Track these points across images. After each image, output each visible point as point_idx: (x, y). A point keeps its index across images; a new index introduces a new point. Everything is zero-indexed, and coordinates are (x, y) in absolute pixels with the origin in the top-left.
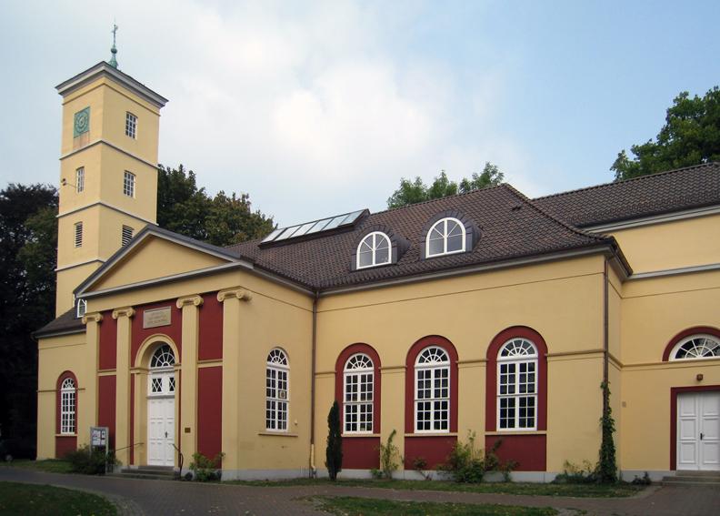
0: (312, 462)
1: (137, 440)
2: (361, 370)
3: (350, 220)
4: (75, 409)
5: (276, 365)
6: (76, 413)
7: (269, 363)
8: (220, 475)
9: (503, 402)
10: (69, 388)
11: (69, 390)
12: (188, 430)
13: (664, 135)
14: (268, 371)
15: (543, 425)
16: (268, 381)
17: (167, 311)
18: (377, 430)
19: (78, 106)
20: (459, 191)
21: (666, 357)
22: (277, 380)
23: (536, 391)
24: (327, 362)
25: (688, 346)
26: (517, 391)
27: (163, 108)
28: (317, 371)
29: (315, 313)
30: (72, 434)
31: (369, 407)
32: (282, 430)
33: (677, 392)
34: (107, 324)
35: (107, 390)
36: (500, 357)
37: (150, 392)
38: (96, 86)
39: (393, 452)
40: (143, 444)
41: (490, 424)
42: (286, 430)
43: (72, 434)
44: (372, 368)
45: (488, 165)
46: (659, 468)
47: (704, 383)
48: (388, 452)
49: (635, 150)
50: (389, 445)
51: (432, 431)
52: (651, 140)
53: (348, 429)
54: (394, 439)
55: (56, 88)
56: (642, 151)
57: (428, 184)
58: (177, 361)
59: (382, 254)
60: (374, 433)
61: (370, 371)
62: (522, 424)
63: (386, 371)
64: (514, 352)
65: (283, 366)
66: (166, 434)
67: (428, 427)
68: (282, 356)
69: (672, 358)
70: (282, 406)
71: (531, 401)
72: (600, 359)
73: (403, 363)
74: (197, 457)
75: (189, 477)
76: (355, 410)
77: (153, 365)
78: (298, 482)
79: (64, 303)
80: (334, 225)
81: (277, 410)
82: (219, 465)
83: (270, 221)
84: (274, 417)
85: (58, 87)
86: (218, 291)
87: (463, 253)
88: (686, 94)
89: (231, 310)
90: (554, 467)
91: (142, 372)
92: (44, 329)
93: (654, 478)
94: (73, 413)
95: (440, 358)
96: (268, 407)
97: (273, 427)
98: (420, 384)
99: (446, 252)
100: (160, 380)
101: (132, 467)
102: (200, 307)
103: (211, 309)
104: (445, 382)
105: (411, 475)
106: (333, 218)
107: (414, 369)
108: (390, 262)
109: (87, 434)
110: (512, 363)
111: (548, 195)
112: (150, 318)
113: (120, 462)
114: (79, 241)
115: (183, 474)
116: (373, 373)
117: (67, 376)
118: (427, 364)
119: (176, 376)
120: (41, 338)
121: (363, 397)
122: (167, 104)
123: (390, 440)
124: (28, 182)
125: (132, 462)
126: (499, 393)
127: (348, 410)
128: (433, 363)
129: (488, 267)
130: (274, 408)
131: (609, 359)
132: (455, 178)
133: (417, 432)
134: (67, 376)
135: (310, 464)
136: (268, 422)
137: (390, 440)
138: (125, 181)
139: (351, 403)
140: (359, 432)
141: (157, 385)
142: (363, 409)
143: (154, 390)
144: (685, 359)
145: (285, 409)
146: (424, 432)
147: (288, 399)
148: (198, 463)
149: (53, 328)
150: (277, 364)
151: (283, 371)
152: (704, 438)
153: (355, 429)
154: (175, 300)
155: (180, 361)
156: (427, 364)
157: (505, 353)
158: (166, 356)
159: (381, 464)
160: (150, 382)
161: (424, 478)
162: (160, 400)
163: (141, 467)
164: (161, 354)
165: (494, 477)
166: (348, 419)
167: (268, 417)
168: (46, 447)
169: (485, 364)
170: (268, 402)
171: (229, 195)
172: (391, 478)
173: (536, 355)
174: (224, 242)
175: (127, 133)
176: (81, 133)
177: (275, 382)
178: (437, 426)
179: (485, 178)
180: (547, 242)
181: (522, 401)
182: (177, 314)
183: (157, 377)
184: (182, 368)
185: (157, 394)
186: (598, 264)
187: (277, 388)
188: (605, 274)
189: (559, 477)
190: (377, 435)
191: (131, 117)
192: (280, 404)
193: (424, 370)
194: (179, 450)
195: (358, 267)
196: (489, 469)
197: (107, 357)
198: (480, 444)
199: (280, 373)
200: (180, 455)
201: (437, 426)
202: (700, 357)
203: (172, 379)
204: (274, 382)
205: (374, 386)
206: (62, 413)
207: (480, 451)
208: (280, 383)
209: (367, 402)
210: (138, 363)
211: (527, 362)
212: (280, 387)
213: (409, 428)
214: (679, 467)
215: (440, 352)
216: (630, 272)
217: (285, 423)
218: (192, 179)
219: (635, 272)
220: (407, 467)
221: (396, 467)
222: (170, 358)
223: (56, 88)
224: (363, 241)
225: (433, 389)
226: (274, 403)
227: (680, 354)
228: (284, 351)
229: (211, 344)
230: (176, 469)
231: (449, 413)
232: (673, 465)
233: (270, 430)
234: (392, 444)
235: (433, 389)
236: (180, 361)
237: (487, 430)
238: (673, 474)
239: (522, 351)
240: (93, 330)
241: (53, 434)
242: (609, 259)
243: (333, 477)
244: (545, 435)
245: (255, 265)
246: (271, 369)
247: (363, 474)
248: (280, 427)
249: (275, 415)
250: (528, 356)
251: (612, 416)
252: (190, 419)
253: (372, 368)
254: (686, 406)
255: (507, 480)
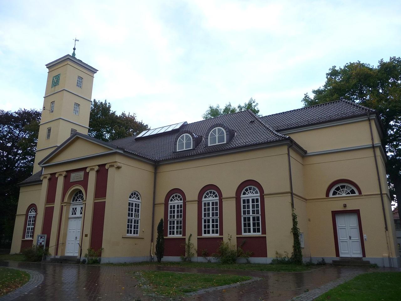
0: (152, 252)
1: (61, 241)
2: (211, 199)
3: (178, 127)
4: (34, 225)
5: (134, 200)
6: (35, 226)
7: (130, 199)
8: (100, 260)
9: (245, 219)
10: (33, 213)
11: (32, 214)
12: (86, 236)
13: (326, 86)
14: (129, 203)
15: (264, 232)
16: (129, 208)
17: (82, 174)
18: (184, 235)
19: (55, 73)
20: (238, 110)
21: (327, 195)
22: (134, 208)
23: (260, 214)
24: (161, 198)
25: (338, 189)
26: (251, 213)
27: (95, 74)
28: (156, 203)
29: (155, 174)
30: (31, 239)
31: (181, 221)
32: (135, 235)
33: (335, 214)
34: (53, 180)
35: (49, 213)
36: (242, 196)
37: (71, 215)
38: (61, 66)
39: (191, 246)
40: (64, 244)
41: (239, 231)
42: (138, 235)
43: (31, 239)
44: (182, 201)
45: (251, 99)
46: (330, 256)
47: (348, 208)
48: (189, 246)
49: (314, 92)
50: (189, 243)
51: (211, 235)
52: (320, 87)
53: (205, 233)
54: (192, 238)
55: (45, 65)
56: (318, 92)
57: (222, 108)
58: (85, 199)
59: (188, 145)
60: (183, 236)
61: (181, 203)
62: (254, 231)
63: (190, 203)
64: (248, 193)
65: (138, 200)
66: (76, 238)
67: (209, 233)
68: (137, 196)
69: (331, 195)
70: (136, 222)
71: (258, 218)
72: (288, 198)
73: (196, 199)
74: (90, 250)
75: (84, 261)
76: (209, 222)
77: (73, 201)
78: (146, 263)
79: (37, 169)
80: (170, 129)
81: (133, 224)
82: (100, 255)
83: (147, 125)
84: (131, 228)
85: (46, 65)
86: (106, 164)
87: (191, 150)
88: (335, 67)
89: (112, 173)
90: (271, 255)
91: (68, 204)
92: (24, 182)
93: (327, 261)
94: (33, 227)
95: (214, 196)
96: (128, 222)
97: (131, 233)
98: (205, 210)
99: (217, 144)
100: (76, 209)
101: (57, 257)
102: (97, 171)
103: (102, 173)
104: (257, 205)
105: (201, 259)
106: (163, 127)
107: (240, 198)
108: (192, 148)
109: (37, 239)
110: (209, 202)
111: (290, 110)
112: (74, 177)
113: (50, 255)
114: (49, 136)
115: (81, 260)
116: (182, 204)
117: (33, 207)
118: (247, 195)
119: (83, 206)
120: (22, 186)
121: (178, 217)
122: (97, 72)
123: (189, 240)
124: (29, 108)
125: (57, 254)
126: (242, 215)
127: (205, 222)
128: (211, 198)
129: (178, 161)
130: (131, 223)
131: (294, 196)
132: (235, 105)
133: (204, 235)
134: (33, 207)
135: (151, 253)
136: (128, 230)
137: (189, 240)
138: (75, 107)
139: (207, 218)
140: (176, 236)
141: (74, 211)
142: (213, 221)
143: (73, 214)
144: (337, 196)
145: (138, 223)
146: (207, 235)
147: (139, 218)
148: (90, 255)
149: (28, 181)
150: (134, 199)
151: (137, 203)
152: (351, 239)
153: (209, 233)
154: (86, 168)
155: (86, 199)
156: (247, 195)
157: (244, 194)
158: (80, 196)
159: (186, 254)
160: (71, 210)
161: (206, 261)
162: (75, 219)
163: (61, 257)
164: (78, 195)
165: (243, 260)
166: (205, 227)
167: (128, 227)
168: (16, 247)
169: (235, 199)
170: (129, 220)
171: (127, 114)
172: (190, 261)
173: (259, 194)
174: (121, 136)
175: (77, 85)
176: (55, 86)
177: (133, 209)
178: (213, 232)
179: (250, 105)
180: (261, 139)
181: (254, 218)
182: (87, 175)
183: (74, 207)
184: (87, 202)
185: (74, 216)
186: (284, 150)
187: (134, 212)
188: (289, 154)
189: (273, 261)
190: (184, 237)
191: (80, 78)
192: (135, 221)
193: (207, 202)
194: (81, 247)
195: (177, 151)
196: (239, 256)
197: (51, 198)
198: (234, 242)
199: (136, 204)
200: (81, 250)
201: (213, 232)
202: (344, 195)
203: (82, 208)
204: (132, 209)
205: (183, 210)
206: (27, 227)
207: (234, 246)
208: (135, 209)
209: (179, 219)
210: (66, 200)
211: (255, 198)
212: (135, 211)
213: (200, 233)
214: (341, 255)
215: (214, 193)
216: (305, 152)
217: (137, 231)
218: (110, 107)
219: (308, 152)
220: (199, 255)
221: (193, 254)
222: (82, 197)
223: (45, 65)
224: (211, 132)
225: (251, 209)
226: (132, 220)
227: (334, 193)
228: (138, 192)
229: (101, 190)
230: (79, 257)
231: (219, 227)
232: (338, 254)
233: (129, 235)
234: (190, 242)
235: (251, 209)
236: (86, 199)
237: (198, 235)
238: (337, 259)
239: (252, 192)
240: (45, 183)
241: (21, 239)
242: (290, 147)
243: (159, 261)
244: (237, 235)
245: (124, 151)
246: (131, 202)
247: (177, 259)
248: (134, 233)
249: (132, 227)
250: (255, 195)
251: (298, 226)
252: (88, 230)
253: (182, 201)
254: (341, 221)
255: (249, 262)
